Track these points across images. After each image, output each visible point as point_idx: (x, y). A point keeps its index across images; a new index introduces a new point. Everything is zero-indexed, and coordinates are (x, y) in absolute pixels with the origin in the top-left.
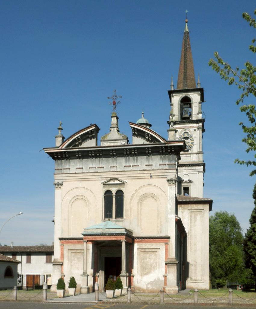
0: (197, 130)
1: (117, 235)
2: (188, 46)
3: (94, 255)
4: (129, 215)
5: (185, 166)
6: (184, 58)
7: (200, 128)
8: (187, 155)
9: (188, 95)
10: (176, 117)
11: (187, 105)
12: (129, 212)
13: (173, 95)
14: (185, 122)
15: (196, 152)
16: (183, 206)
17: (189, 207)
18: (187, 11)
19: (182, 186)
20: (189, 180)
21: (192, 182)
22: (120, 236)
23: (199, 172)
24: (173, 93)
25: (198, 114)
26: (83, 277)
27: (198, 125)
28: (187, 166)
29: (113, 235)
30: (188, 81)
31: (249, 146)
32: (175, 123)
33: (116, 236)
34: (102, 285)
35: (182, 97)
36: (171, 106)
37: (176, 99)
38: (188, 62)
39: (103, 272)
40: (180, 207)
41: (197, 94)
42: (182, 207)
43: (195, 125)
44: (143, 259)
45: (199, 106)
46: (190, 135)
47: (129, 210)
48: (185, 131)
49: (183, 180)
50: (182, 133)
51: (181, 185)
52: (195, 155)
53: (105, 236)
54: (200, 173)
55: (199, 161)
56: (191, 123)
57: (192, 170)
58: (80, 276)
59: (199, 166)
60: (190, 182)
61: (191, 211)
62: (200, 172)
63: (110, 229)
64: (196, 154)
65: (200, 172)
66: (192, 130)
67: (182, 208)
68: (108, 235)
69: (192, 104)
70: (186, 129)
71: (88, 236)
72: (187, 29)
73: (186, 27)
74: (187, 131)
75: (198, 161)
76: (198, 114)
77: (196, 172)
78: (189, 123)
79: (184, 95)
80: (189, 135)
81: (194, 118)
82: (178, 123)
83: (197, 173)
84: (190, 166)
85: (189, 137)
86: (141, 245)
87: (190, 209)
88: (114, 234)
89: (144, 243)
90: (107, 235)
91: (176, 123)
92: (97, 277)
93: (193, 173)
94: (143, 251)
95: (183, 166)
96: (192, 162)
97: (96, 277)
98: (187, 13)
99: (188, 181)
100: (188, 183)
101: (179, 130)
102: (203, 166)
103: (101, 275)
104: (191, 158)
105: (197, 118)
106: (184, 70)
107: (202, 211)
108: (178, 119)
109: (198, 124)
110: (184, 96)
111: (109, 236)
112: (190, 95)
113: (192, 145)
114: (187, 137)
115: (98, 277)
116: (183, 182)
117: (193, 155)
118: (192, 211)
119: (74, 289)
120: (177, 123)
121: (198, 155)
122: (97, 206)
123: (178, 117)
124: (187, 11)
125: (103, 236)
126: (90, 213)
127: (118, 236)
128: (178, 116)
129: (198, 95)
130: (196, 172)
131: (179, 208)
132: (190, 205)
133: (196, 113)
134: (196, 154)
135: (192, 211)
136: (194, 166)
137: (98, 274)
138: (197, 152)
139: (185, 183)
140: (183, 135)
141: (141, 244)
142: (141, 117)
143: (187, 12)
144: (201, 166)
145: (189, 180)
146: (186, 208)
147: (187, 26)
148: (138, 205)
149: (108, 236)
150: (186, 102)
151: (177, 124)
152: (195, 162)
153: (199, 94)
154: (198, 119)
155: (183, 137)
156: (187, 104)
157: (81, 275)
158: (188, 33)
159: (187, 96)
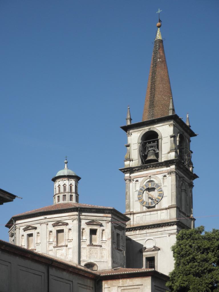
0: (167, 176)
2: (159, 60)
5: (148, 229)
6: (152, 77)
7: (172, 172)
8: (152, 213)
9: (154, 128)
10: (136, 161)
11: (153, 143)
13: (131, 131)
14: (148, 168)
15: (167, 206)
16: (110, 282)
17: (119, 282)
18: (159, 11)
19: (144, 256)
20: (154, 247)
21: (159, 249)
23: (170, 234)
24: (131, 130)
25: (169, 153)
27: (168, 168)
28: (151, 228)
30: (156, 108)
31: (69, 180)
32: (131, 170)
35: (144, 132)
36: (127, 148)
37: (135, 138)
38: (157, 83)
40: (105, 284)
41: (168, 125)
42: (109, 283)
43: (165, 169)
45: (171, 141)
46: (157, 184)
48: (149, 180)
49: (145, 248)
50: (145, 183)
51: (143, 255)
52: (164, 211)
54: (171, 236)
55: (170, 219)
56: (158, 167)
57: (159, 233)
59: (170, 225)
60: (157, 249)
61: (123, 288)
62: (172, 234)
64: (166, 209)
65: (172, 234)
66: (160, 176)
67: (109, 285)
69: (160, 141)
70: (150, 177)
72: (159, 37)
73: (158, 33)
74: (152, 179)
75: (169, 219)
76: (169, 153)
77: (165, 235)
78: (154, 168)
79: (146, 129)
80: (154, 184)
81: (163, 158)
82: (137, 169)
83: (167, 235)
84: (156, 227)
85: (154, 187)
87: (121, 286)
91: (134, 169)
93: (161, 236)
95: (145, 229)
96: (161, 221)
98: (159, 14)
99: (154, 249)
100: (153, 251)
101: (140, 180)
102: (176, 224)
104: (157, 215)
105: (168, 159)
106: (151, 94)
107: (140, 287)
108: (138, 165)
109: (170, 167)
110: (148, 130)
112: (156, 128)
113: (160, 198)
114: (153, 187)
116: (146, 250)
117: (162, 211)
118: (125, 288)
120: (136, 170)
121: (169, 210)
123: (138, 162)
124: (159, 11)
128: (138, 161)
129: (169, 125)
130: (165, 235)
131: (105, 285)
132: (121, 281)
133: (167, 152)
134: (166, 209)
135: (125, 288)
136: (162, 226)
138: (167, 207)
139: (148, 251)
140: (146, 185)
142: (64, 168)
143: (160, 12)
144: (173, 225)
145: (154, 247)
146: (114, 284)
147: (159, 31)
150: (151, 139)
151: (136, 171)
152: (164, 220)
153: (171, 124)
154: (169, 159)
155: (145, 188)
156: (154, 142)
158: (161, 41)
159: (152, 129)
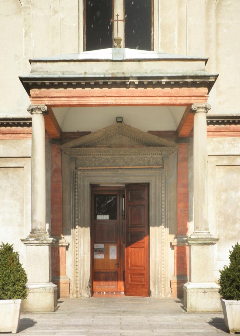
1: (177, 85)
3: (49, 175)
4: (176, 44)
12: (176, 33)
22: (185, 91)
26: (34, 248)
29: (159, 85)
33: (167, 90)
34: (84, 273)
39: (87, 230)
44: (226, 191)
47: (176, 29)
53: (123, 89)
58: (22, 244)
63: (144, 63)
68: (137, 82)
71: (52, 90)
86: (220, 142)
88: (164, 81)
89: (230, 138)
90: (132, 84)
92: (62, 250)
94: (225, 163)
97: (61, 249)
103: (78, 244)
111: (141, 89)
115: (67, 248)
119: (19, 301)
122: (56, 12)
125: (114, 89)
126: (31, 34)
127: (176, 89)
137: (66, 240)
141: (220, 139)
148: (208, 10)
149: (137, 86)
157: (22, 240)
